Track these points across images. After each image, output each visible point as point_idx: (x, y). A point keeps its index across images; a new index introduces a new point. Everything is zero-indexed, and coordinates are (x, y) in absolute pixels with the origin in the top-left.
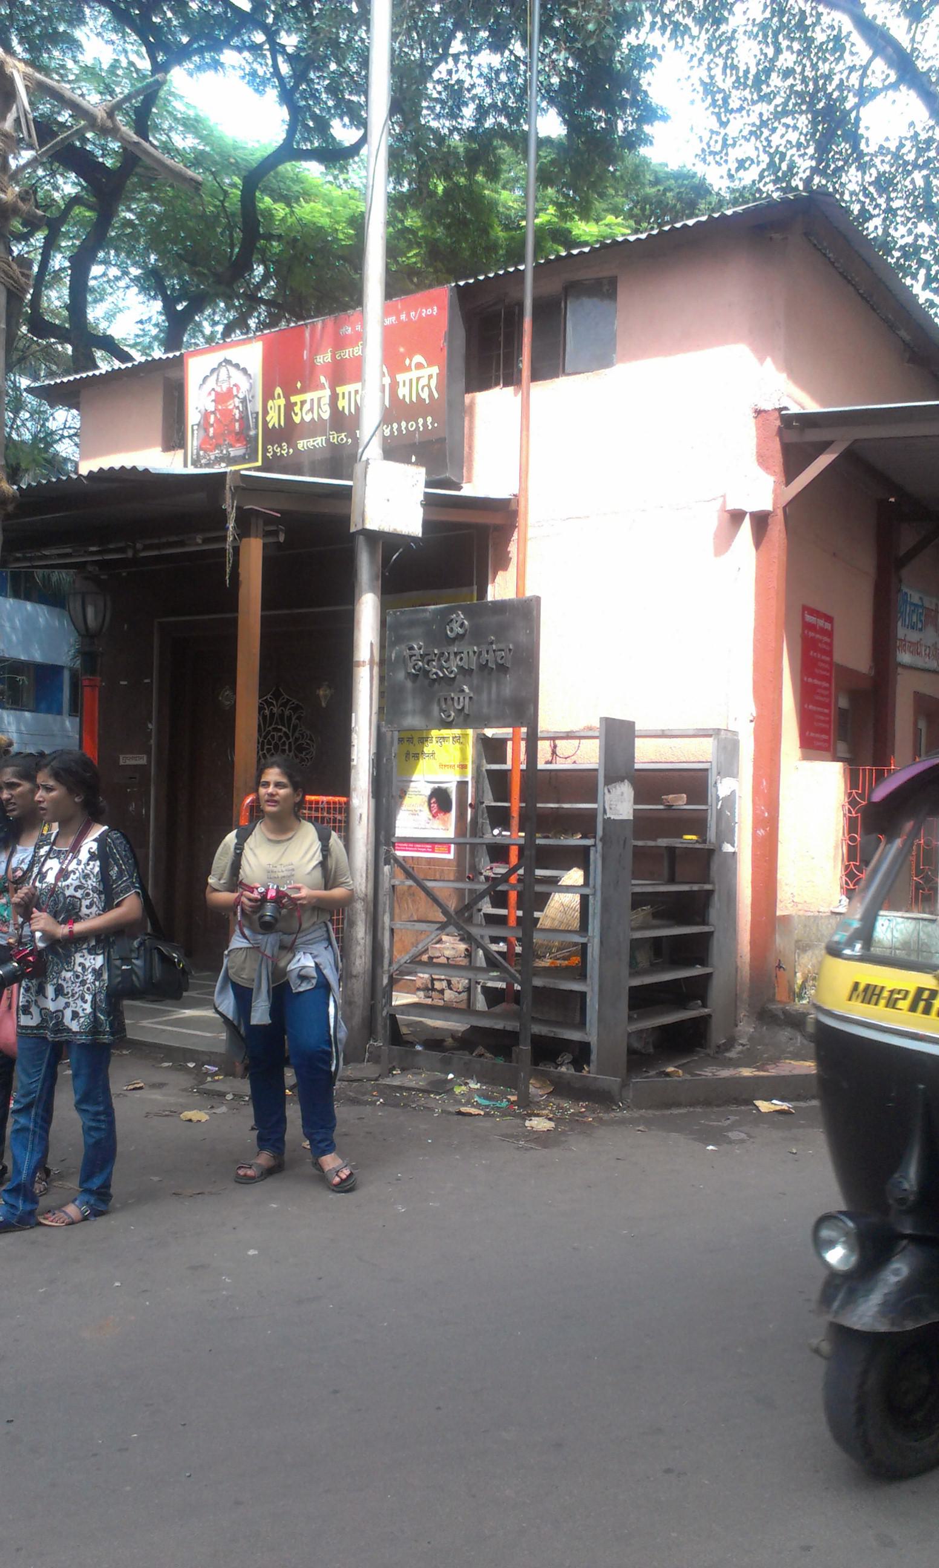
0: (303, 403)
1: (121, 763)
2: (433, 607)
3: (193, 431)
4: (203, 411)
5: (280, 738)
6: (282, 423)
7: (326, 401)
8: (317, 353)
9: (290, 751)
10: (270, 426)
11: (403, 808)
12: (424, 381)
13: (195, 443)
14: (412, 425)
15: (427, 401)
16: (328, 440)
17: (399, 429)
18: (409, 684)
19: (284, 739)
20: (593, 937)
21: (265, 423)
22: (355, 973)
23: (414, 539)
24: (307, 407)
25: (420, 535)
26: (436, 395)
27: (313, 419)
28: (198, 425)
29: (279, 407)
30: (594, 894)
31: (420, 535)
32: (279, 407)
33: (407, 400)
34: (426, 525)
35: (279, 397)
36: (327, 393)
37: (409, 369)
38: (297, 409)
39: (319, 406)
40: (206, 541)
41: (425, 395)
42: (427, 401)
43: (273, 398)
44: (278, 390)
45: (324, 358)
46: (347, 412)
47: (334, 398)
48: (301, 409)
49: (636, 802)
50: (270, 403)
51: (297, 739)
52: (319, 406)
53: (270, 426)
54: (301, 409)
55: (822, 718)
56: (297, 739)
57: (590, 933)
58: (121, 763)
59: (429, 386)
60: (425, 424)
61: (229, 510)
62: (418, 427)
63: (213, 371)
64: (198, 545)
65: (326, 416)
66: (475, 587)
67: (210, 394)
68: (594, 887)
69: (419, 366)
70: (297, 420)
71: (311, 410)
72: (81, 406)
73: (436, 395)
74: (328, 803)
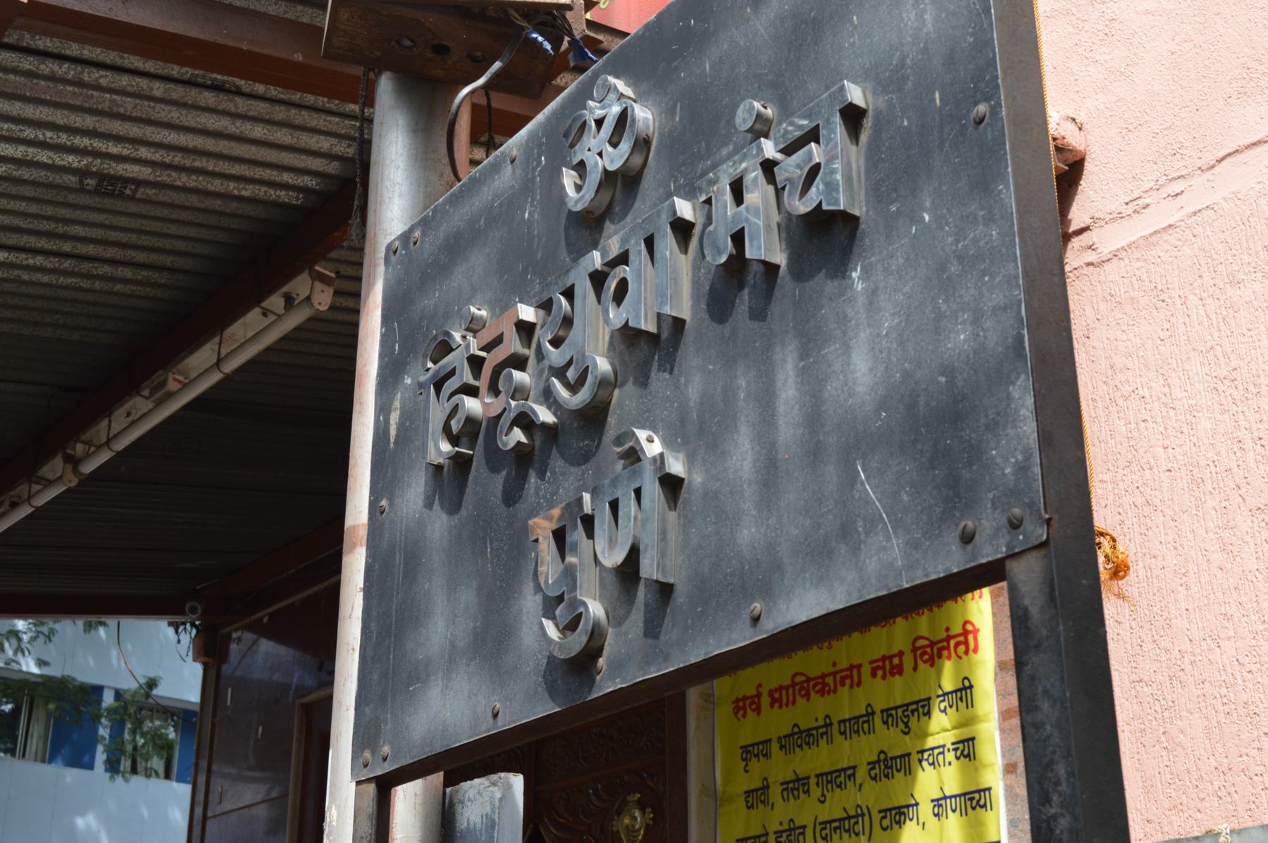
18: (439, 525)
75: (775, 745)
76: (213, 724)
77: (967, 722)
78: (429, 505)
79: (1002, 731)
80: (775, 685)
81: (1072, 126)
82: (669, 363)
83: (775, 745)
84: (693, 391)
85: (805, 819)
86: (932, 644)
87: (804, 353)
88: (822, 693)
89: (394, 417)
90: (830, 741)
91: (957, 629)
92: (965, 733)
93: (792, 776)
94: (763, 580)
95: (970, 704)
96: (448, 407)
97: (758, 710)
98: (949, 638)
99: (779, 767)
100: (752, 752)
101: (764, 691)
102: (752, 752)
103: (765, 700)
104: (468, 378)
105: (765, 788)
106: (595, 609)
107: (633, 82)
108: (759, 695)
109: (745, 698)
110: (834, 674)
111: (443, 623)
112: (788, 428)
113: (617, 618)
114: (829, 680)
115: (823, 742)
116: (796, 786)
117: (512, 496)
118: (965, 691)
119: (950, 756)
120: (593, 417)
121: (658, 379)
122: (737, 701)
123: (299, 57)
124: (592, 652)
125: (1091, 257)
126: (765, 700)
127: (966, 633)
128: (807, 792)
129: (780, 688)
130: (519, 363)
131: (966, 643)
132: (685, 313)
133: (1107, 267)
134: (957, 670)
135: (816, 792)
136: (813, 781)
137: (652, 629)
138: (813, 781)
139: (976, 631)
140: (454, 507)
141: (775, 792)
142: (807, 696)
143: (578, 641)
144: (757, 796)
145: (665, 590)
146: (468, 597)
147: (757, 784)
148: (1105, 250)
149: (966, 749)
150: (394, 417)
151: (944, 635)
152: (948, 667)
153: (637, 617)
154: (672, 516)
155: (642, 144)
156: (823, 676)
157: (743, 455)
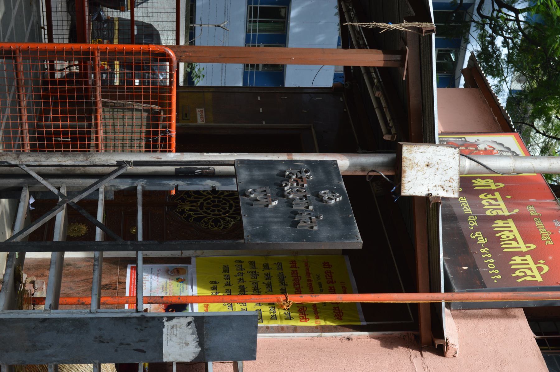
0: (496, 200)
1: (197, 110)
2: (344, 184)
3: (461, 138)
4: (476, 143)
5: (225, 209)
6: (476, 188)
7: (500, 213)
8: (535, 206)
9: (213, 215)
10: (474, 181)
11: (168, 281)
12: (528, 272)
13: (450, 139)
14: (491, 266)
15: (513, 275)
16: (470, 215)
17: (487, 258)
18: (275, 172)
19: (223, 211)
20: (50, 313)
21: (475, 178)
22: (21, 156)
23: (399, 189)
24: (493, 202)
25: (403, 194)
26: (519, 281)
27: (484, 206)
28: (466, 141)
29: (490, 186)
30: (91, 312)
31: (403, 194)
32: (490, 186)
33: (512, 262)
34: (411, 198)
35: (496, 186)
36: (507, 213)
37: (536, 262)
38: (490, 196)
39: (494, 209)
40: (378, 99)
41: (517, 273)
42: (513, 275)
43: (495, 182)
44: (502, 185)
45: (532, 211)
46: (494, 225)
47: (503, 218)
48: (490, 199)
49: (178, 364)
50: (491, 181)
51: (224, 219)
52: (494, 209)
53: (474, 181)
54: (490, 199)
55: (276, 220)
56: (224, 219)
57: (52, 311)
58: (197, 110)
59: (526, 275)
60: (494, 274)
61: (403, 25)
62: (491, 270)
63: (509, 149)
64: (374, 94)
65: (488, 213)
66: (365, 323)
67: (490, 147)
68: (97, 312)
69: (540, 269)
70: (482, 196)
71: (491, 204)
72: (468, 89)
73: (519, 281)
74: (170, 138)
75: (280, 271)
76: (309, 93)
77: (281, 318)
78: (280, 171)
79: (278, 326)
80: (298, 271)
81: (453, 352)
82: (288, 206)
83: (280, 271)
84: (282, 209)
85: (258, 279)
86: (304, 311)
87: (281, 222)
88: (294, 284)
89: (299, 164)
90: (280, 285)
91: (307, 317)
92: (278, 318)
93: (271, 275)
94: (250, 215)
95: (286, 319)
96: (295, 173)
97: (292, 267)
98: (305, 315)
99: (274, 273)
100: (280, 266)
101: (297, 269)
102: (280, 266)
103: (294, 269)
104: (298, 176)
105: (269, 269)
106: (252, 196)
107: (340, 201)
108: (296, 267)
109: (295, 264)
110: (299, 287)
111: (258, 174)
112: (270, 219)
113: (251, 199)
114: (298, 286)
115: (280, 284)
116: (268, 277)
117: (276, 184)
118: (290, 318)
119: (272, 314)
120: (283, 196)
121: (285, 204)
122: (295, 261)
123: (413, 134)
124: (246, 196)
125: (413, 356)
126: (294, 269)
127: (306, 319)
128: (266, 279)
129: (297, 273)
130: (298, 184)
131: (303, 319)
132: (294, 208)
133: (409, 360)
134: (296, 316)
135: (266, 282)
136: (269, 281)
137: (247, 203)
138: (269, 281)
139: (306, 321)
140: (277, 175)
141: (268, 271)
142: (294, 280)
143: (248, 194)
144: (266, 266)
145: (252, 205)
146: (261, 178)
147: (270, 266)
148: (415, 360)
149: (274, 318)
150: (299, 164)
151: (306, 313)
152: (297, 314)
153: (250, 202)
154: (263, 206)
155: (326, 202)
156: (299, 284)
157: (268, 214)
